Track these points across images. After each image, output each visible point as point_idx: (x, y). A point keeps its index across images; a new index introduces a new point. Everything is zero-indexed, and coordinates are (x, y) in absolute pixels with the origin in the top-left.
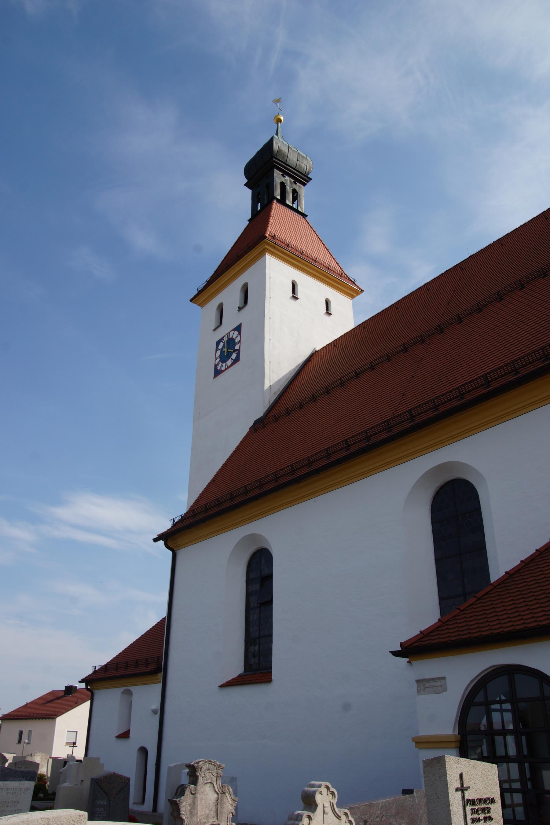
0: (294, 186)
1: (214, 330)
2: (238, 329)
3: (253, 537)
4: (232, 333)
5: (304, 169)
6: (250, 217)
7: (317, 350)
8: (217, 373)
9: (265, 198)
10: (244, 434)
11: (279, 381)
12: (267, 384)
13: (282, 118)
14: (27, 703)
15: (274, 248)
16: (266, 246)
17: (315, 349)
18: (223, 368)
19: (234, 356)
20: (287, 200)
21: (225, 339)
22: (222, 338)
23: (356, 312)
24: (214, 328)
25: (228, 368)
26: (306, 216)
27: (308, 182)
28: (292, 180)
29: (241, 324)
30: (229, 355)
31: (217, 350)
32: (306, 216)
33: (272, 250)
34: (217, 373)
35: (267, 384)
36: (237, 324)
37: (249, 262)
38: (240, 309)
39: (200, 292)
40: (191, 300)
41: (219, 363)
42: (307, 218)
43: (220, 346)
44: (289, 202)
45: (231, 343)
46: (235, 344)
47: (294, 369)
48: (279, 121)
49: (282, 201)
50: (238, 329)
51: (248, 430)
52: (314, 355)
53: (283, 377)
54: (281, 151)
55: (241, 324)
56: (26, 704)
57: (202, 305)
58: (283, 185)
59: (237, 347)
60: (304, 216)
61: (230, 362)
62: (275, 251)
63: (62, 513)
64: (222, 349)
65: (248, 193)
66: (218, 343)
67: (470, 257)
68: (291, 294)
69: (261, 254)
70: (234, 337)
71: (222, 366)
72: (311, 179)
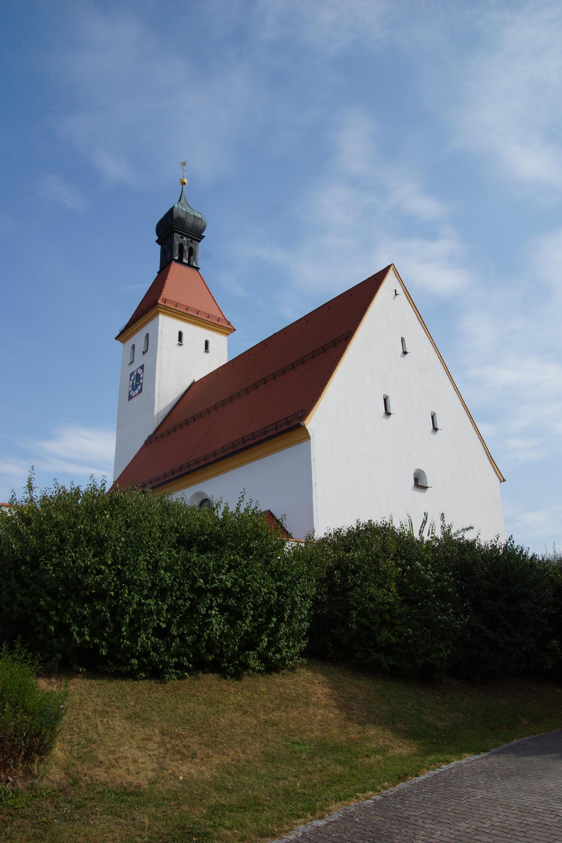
0: (191, 245)
1: (130, 364)
2: (142, 367)
3: (199, 494)
4: (139, 369)
5: (199, 228)
6: (159, 270)
7: (196, 381)
8: (130, 397)
9: (168, 256)
10: (141, 446)
11: (165, 408)
12: (156, 411)
13: (186, 181)
15: (165, 309)
16: (159, 309)
17: (194, 380)
18: (133, 395)
19: (139, 387)
20: (184, 258)
21: (135, 373)
22: (133, 372)
23: (230, 348)
24: (129, 363)
25: (136, 395)
26: (199, 269)
27: (202, 239)
28: (189, 240)
29: (144, 365)
30: (137, 386)
31: (130, 381)
32: (199, 269)
33: (164, 311)
34: (130, 397)
35: (156, 411)
36: (142, 364)
37: (149, 319)
38: (144, 353)
39: (122, 333)
40: (116, 338)
41: (131, 391)
42: (199, 270)
43: (132, 378)
44: (185, 261)
45: (138, 377)
46: (140, 379)
47: (177, 398)
48: (184, 183)
49: (180, 261)
50: (142, 367)
51: (143, 443)
52: (193, 384)
53: (168, 405)
54: (180, 217)
55: (144, 365)
57: (123, 342)
58: (181, 246)
59: (141, 381)
60: (197, 269)
61: (137, 391)
62: (166, 311)
63: (52, 447)
64: (133, 380)
65: (159, 247)
66: (131, 375)
67: (274, 334)
68: (178, 342)
69: (156, 314)
70: (140, 373)
71: (133, 393)
72: (204, 237)
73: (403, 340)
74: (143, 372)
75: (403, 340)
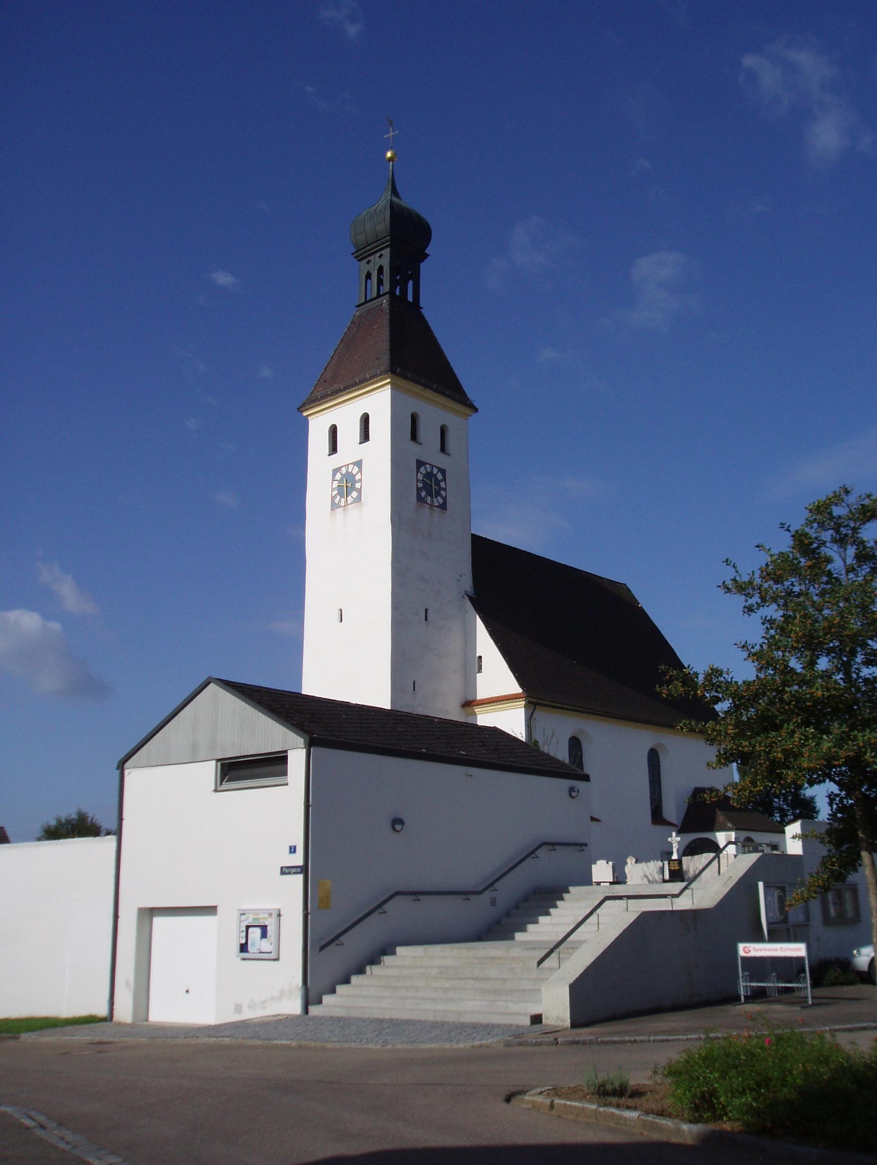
14: (422, 308)
21: (344, 470)
31: (333, 480)
56: (421, 306)
73: (414, 682)
74: (360, 471)
75: (414, 682)
